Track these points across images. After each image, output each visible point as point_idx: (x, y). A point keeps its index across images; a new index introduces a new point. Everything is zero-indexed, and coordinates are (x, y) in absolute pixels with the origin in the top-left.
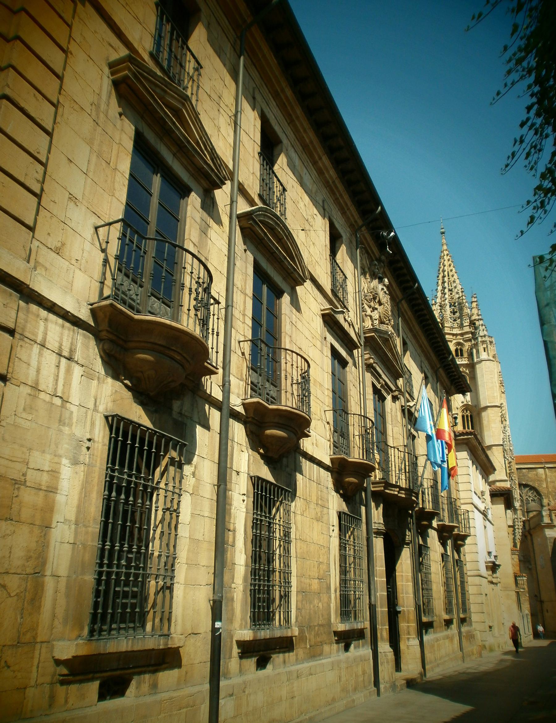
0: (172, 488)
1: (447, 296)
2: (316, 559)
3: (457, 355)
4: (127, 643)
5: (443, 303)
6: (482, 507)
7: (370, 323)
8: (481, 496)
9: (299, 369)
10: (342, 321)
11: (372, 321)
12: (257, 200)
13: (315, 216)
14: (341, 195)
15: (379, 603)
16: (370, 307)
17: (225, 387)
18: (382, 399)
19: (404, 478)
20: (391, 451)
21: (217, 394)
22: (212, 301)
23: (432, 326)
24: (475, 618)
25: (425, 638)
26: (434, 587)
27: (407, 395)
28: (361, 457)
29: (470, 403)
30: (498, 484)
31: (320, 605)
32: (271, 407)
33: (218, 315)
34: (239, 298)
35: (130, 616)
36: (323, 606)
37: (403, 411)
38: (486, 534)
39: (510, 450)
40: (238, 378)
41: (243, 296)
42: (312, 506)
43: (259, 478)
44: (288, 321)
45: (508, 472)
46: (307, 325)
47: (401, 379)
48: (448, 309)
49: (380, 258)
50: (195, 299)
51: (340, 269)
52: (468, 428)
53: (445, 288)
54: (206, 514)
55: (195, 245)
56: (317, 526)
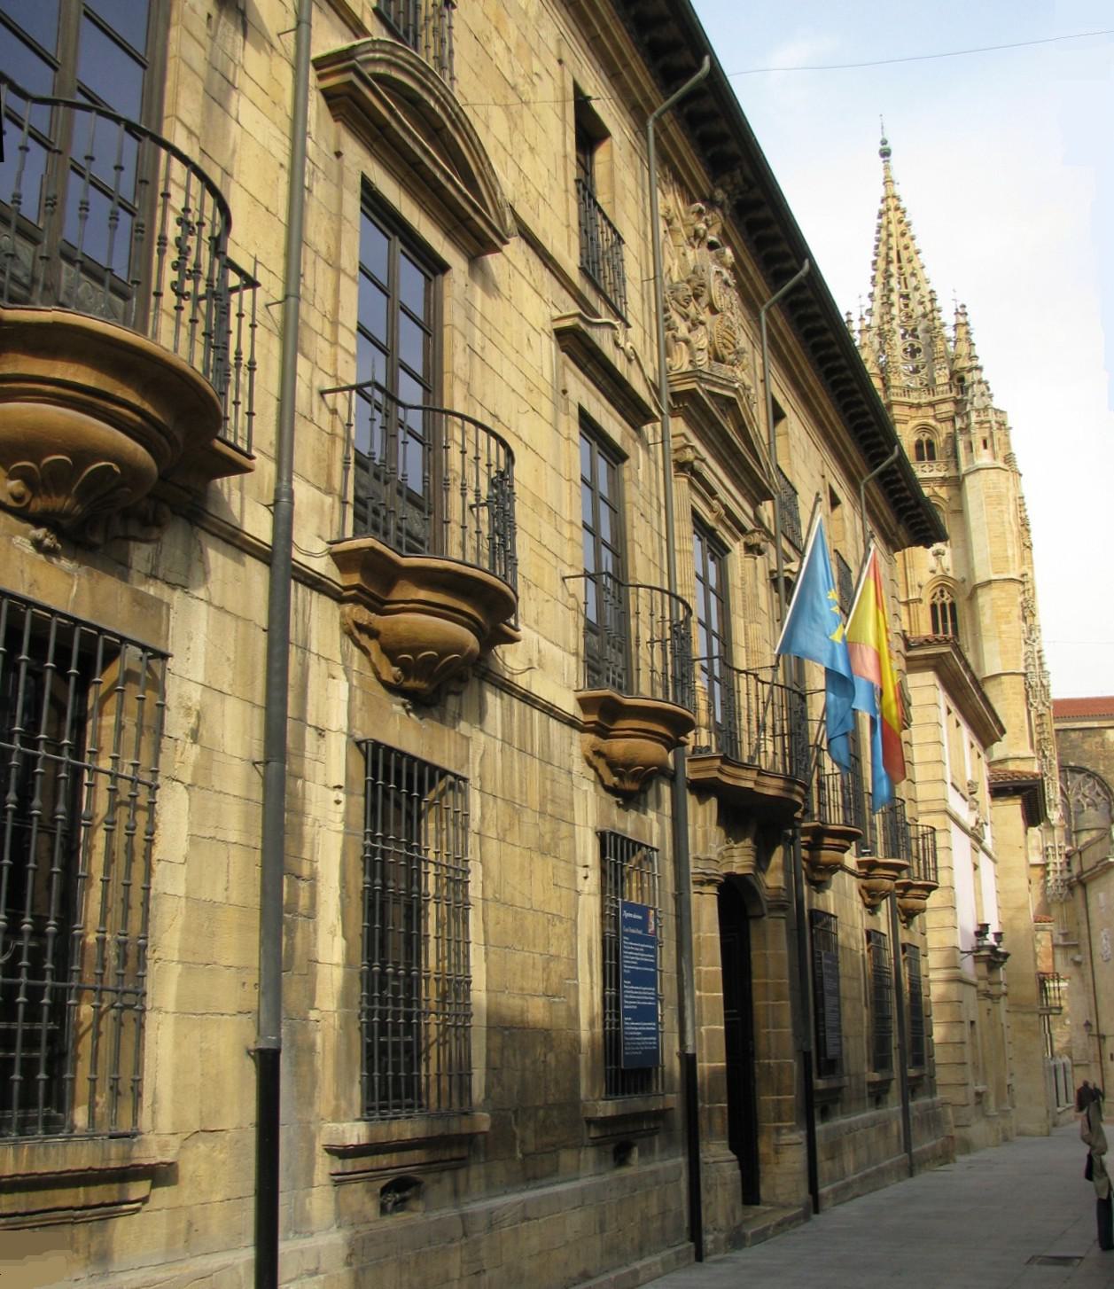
0: (131, 768)
1: (895, 311)
2: (539, 949)
3: (920, 458)
4: (16, 1157)
5: (886, 327)
6: (968, 819)
7: (686, 359)
8: (967, 795)
9: (483, 463)
10: (608, 349)
11: (692, 354)
12: (370, 22)
13: (535, 79)
14: (605, 28)
15: (704, 1051)
16: (686, 317)
17: (282, 510)
18: (717, 550)
19: (770, 748)
20: (742, 683)
21: (259, 525)
22: (234, 280)
23: (876, 428)
24: (942, 1075)
25: (819, 1127)
26: (847, 1010)
27: (785, 544)
28: (660, 695)
29: (950, 574)
30: (1012, 766)
31: (551, 1058)
32: (405, 562)
33: (253, 316)
34: (320, 279)
35: (21, 1088)
36: (557, 1061)
37: (775, 582)
38: (977, 879)
39: (1043, 686)
40: (318, 488)
41: (330, 274)
42: (529, 817)
43: (377, 745)
44: (460, 343)
45: (1036, 737)
46: (514, 356)
47: (768, 504)
48: (899, 343)
49: (712, 194)
50: (177, 266)
51: (605, 217)
52: (945, 631)
53: (891, 290)
54: (233, 836)
55: (191, 132)
56: (543, 868)
